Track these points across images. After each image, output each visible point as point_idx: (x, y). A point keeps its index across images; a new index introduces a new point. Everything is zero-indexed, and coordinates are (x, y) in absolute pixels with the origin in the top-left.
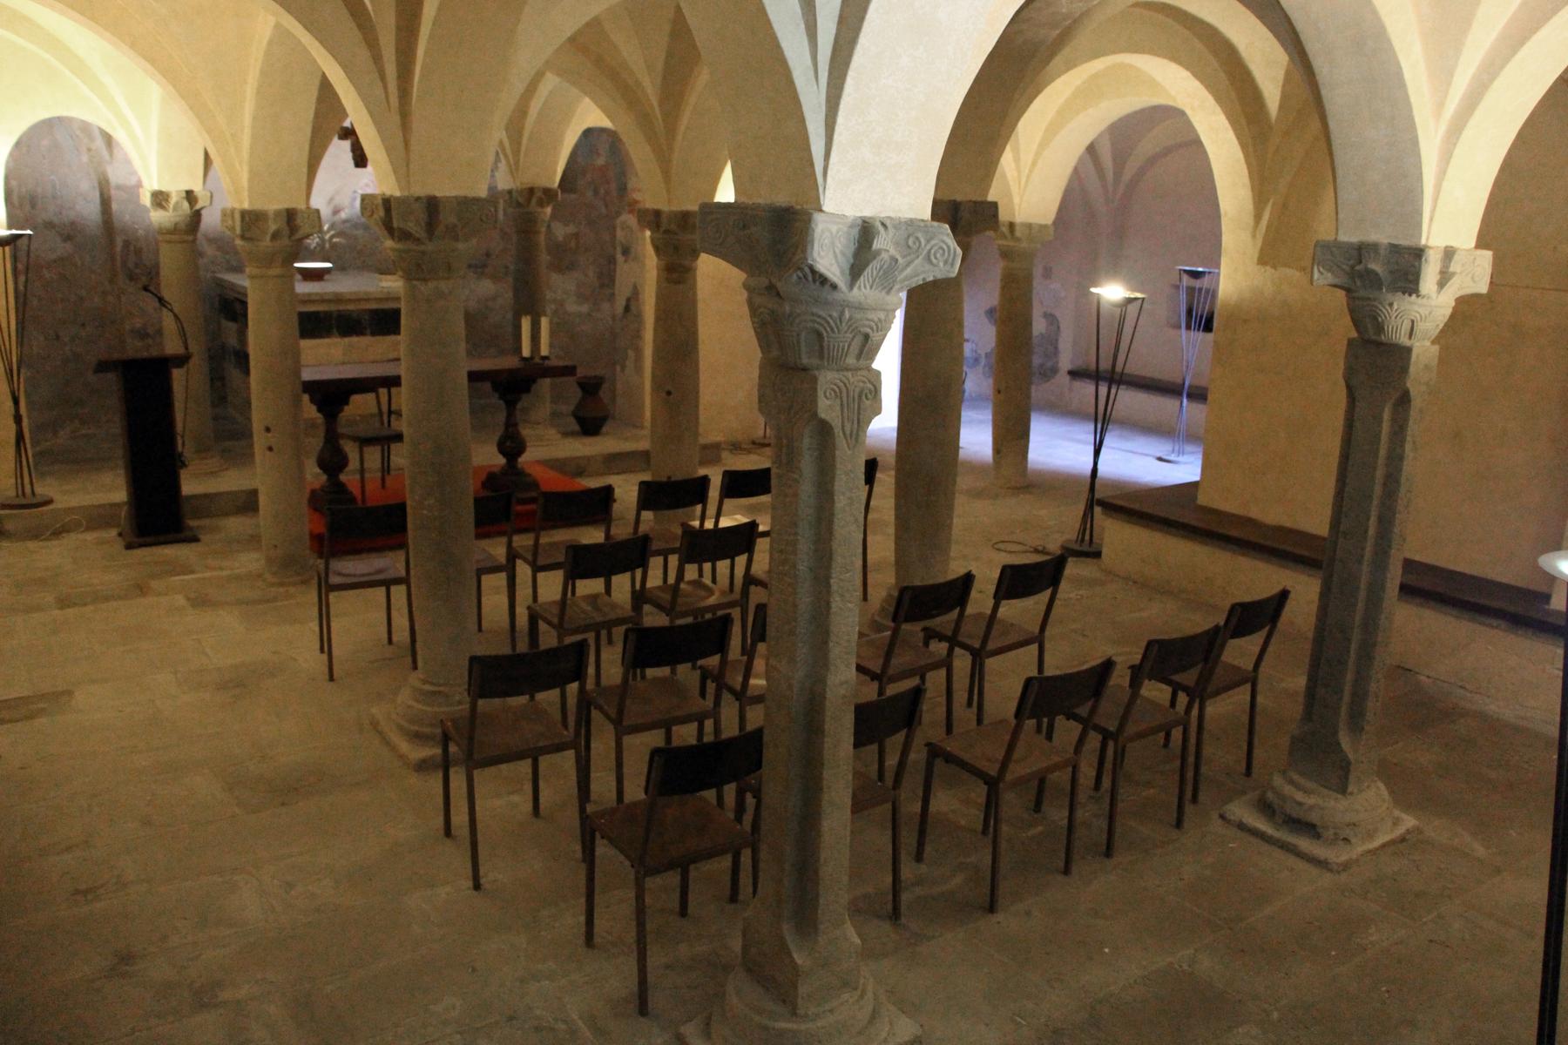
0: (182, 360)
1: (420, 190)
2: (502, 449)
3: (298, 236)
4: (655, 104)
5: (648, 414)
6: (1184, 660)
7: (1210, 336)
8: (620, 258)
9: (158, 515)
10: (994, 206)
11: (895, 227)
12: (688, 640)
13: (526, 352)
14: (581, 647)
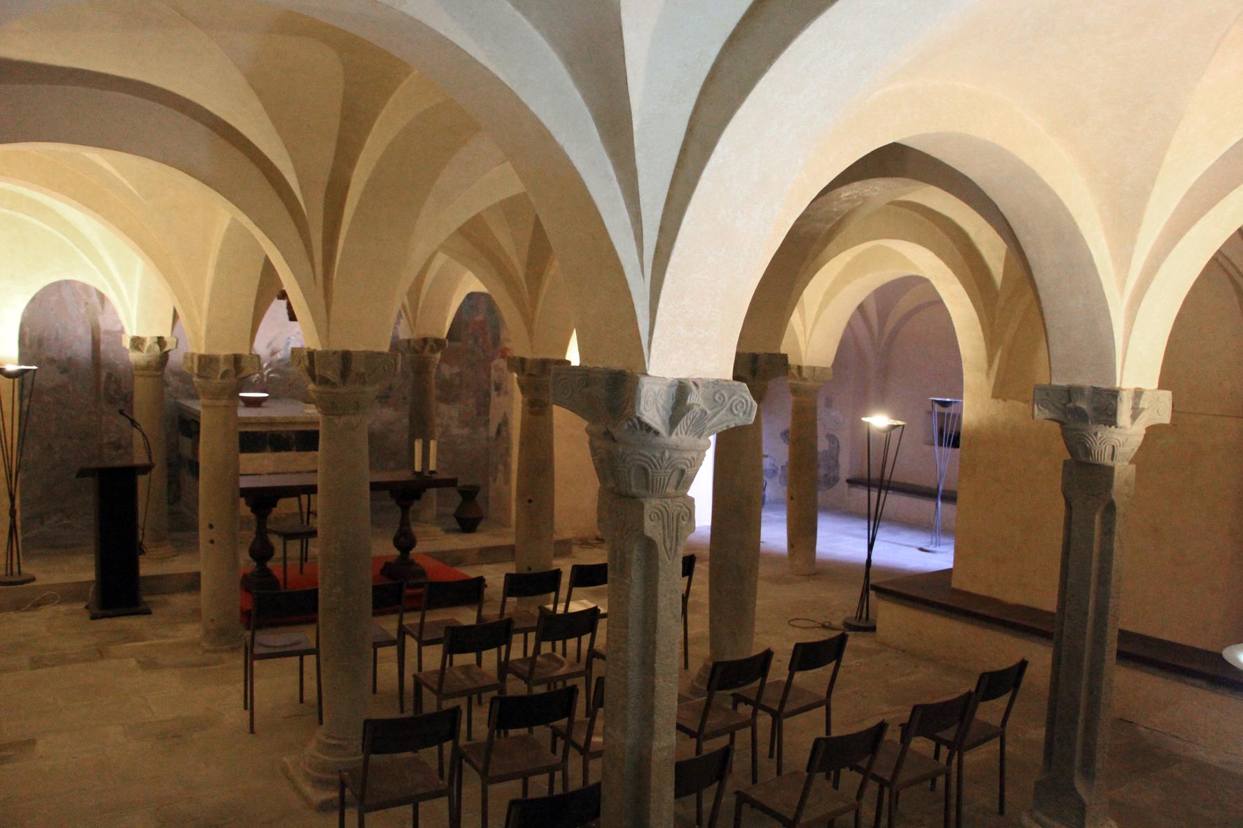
0: (146, 469)
1: (340, 344)
2: (397, 543)
3: (243, 374)
4: (523, 278)
5: (513, 516)
6: (944, 720)
7: (958, 450)
8: (494, 393)
9: (119, 592)
10: (785, 357)
11: (704, 386)
12: (539, 707)
13: (418, 468)
14: (456, 711)
